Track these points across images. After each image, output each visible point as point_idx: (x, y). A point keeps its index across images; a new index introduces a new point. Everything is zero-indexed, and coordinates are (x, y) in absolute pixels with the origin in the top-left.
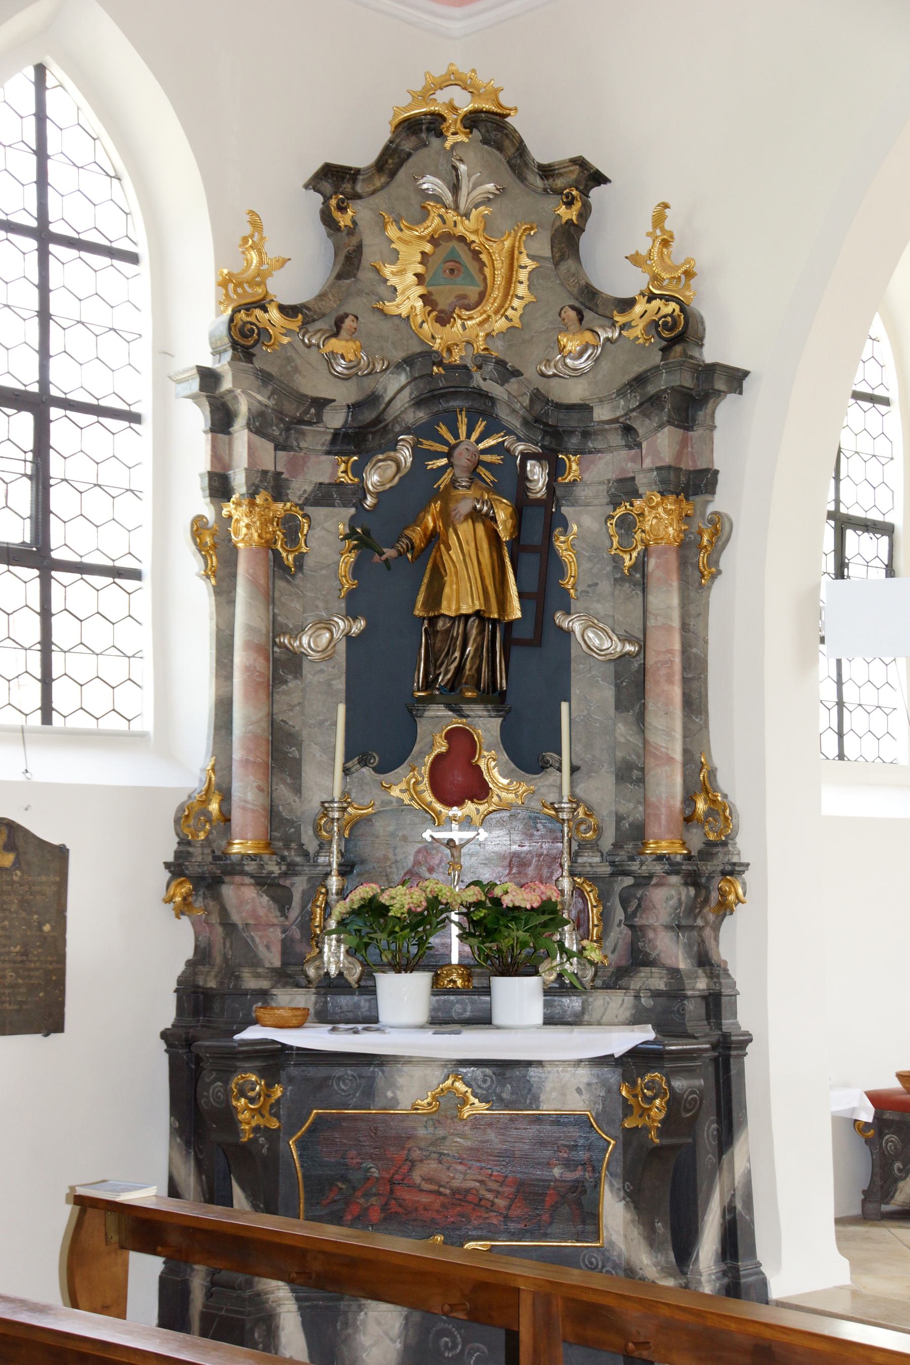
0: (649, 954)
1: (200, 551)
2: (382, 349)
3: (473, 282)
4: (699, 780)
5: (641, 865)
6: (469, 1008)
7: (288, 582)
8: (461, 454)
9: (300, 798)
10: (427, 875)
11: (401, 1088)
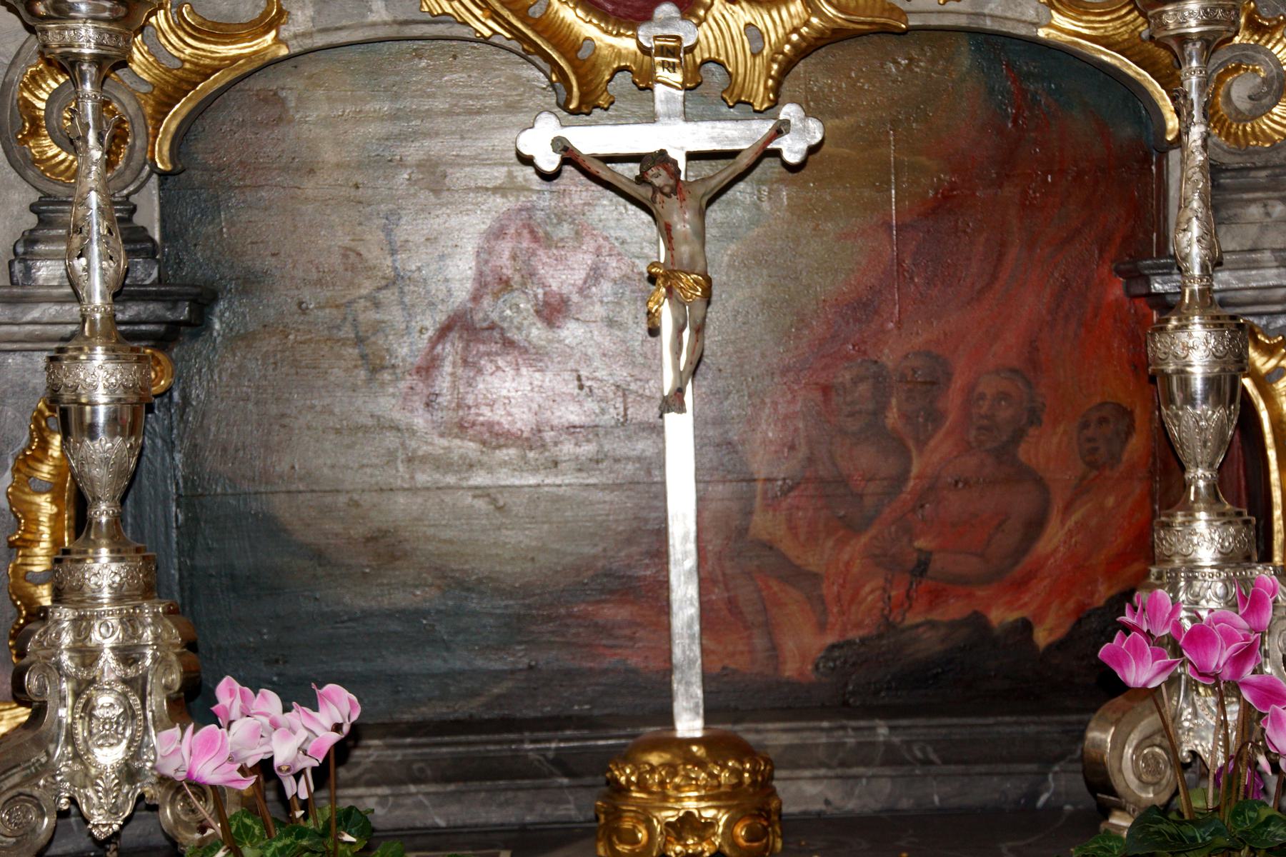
10: (537, 332)
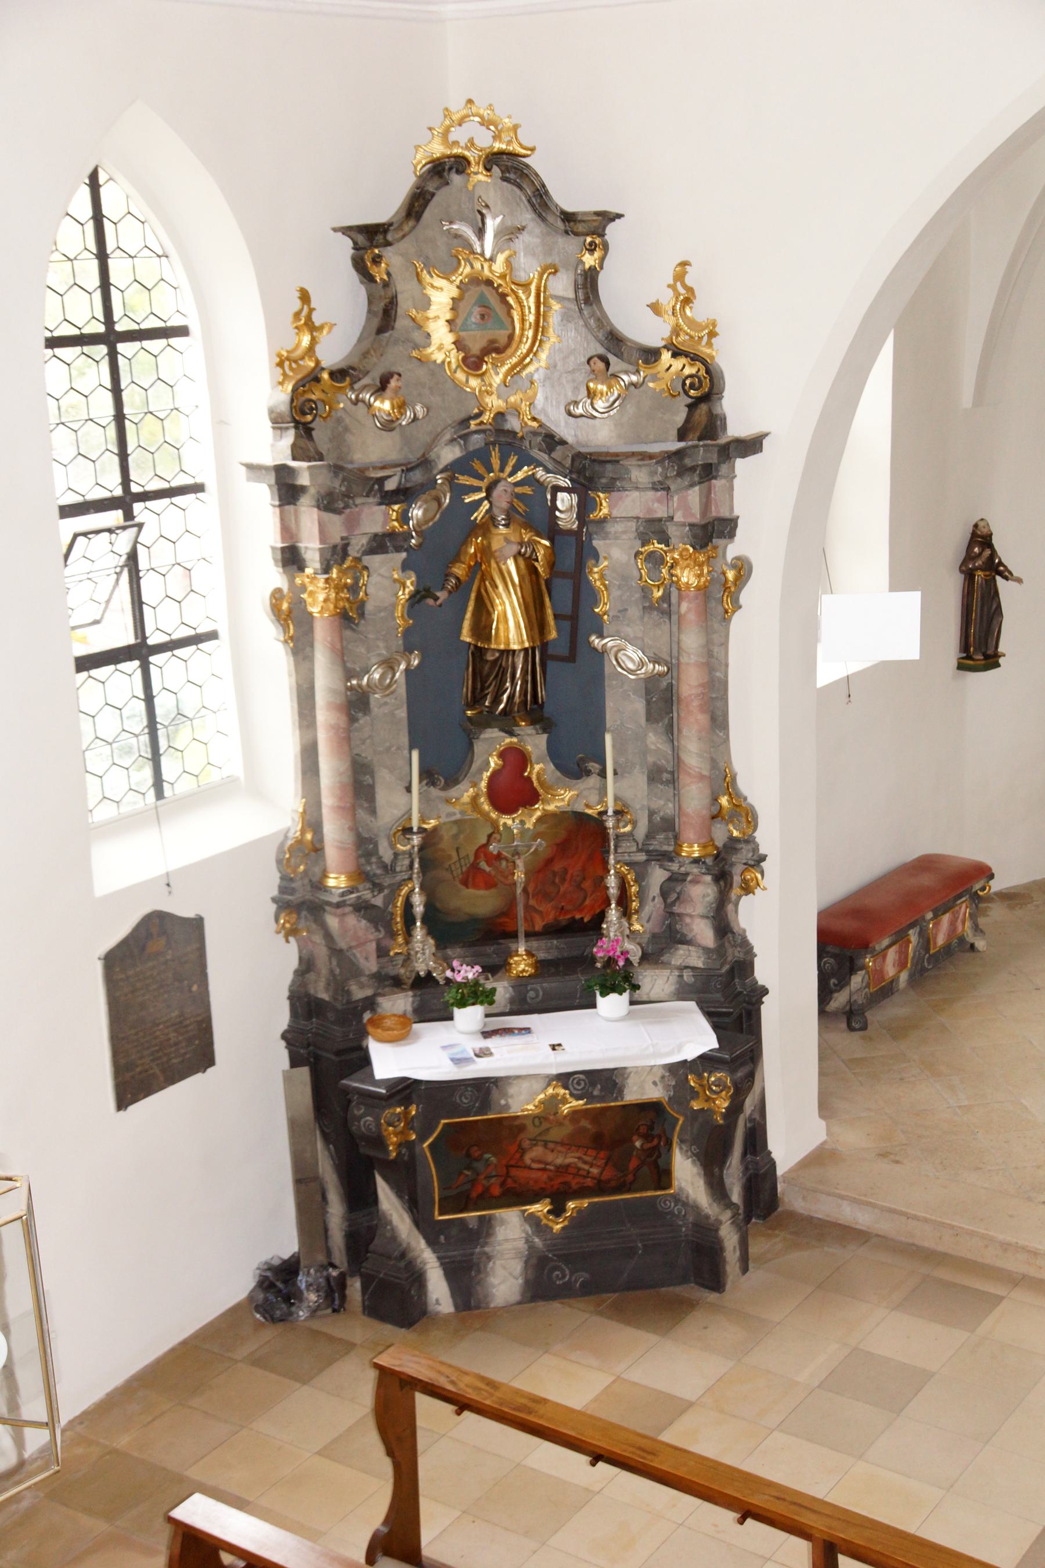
0: (686, 935)
1: (278, 620)
2: (420, 395)
3: (502, 326)
4: (723, 780)
5: (680, 866)
6: (541, 993)
7: (353, 630)
8: (500, 496)
9: (376, 818)
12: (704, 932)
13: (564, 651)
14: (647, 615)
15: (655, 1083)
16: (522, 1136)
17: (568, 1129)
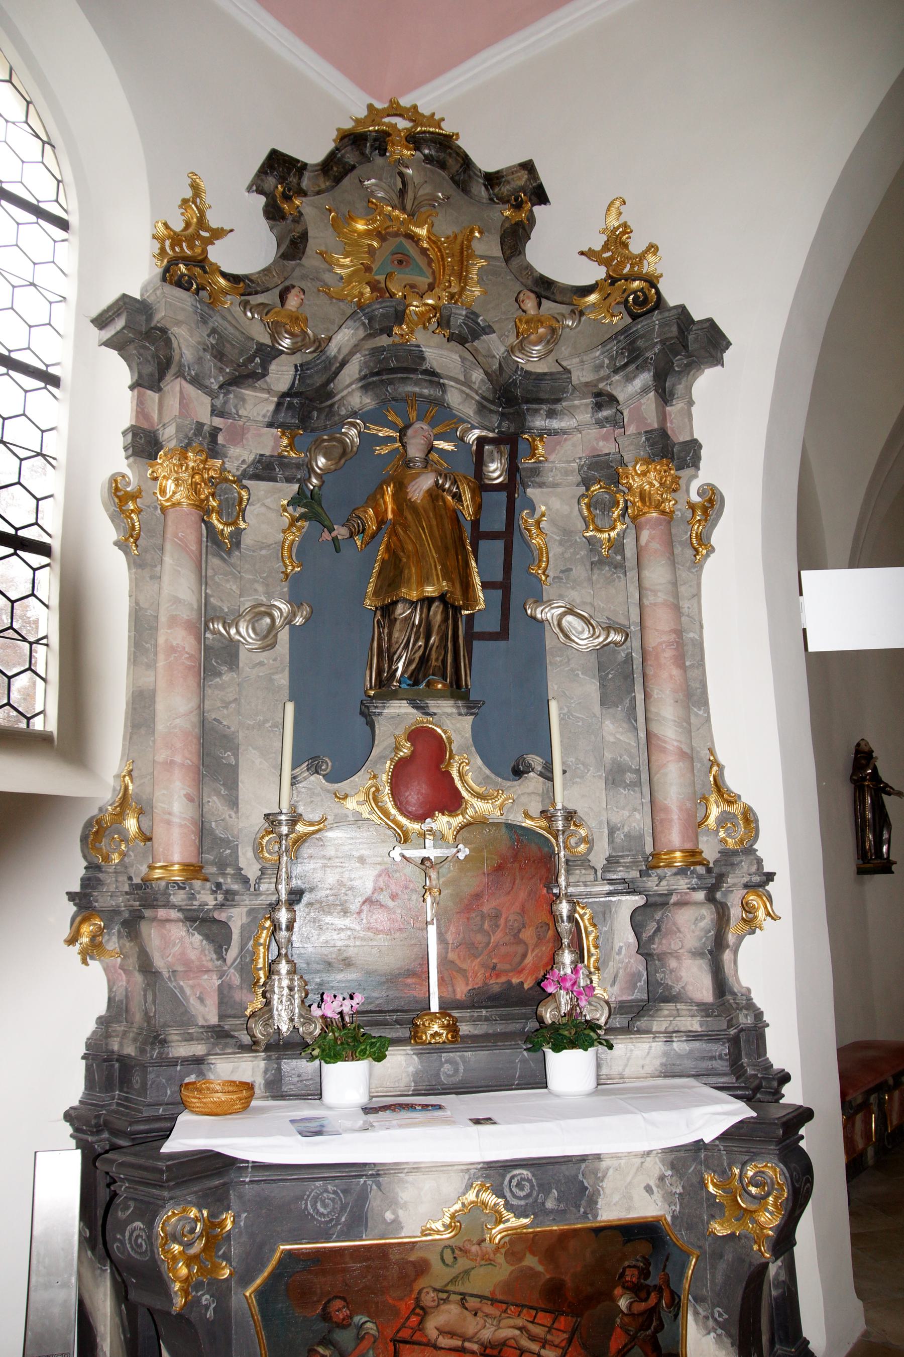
0: (671, 987)
6: (461, 1068)
9: (237, 812)
11: (405, 1206)
12: (695, 980)
13: (494, 626)
14: (596, 571)
15: (649, 1189)
16: (421, 1283)
17: (503, 1270)
